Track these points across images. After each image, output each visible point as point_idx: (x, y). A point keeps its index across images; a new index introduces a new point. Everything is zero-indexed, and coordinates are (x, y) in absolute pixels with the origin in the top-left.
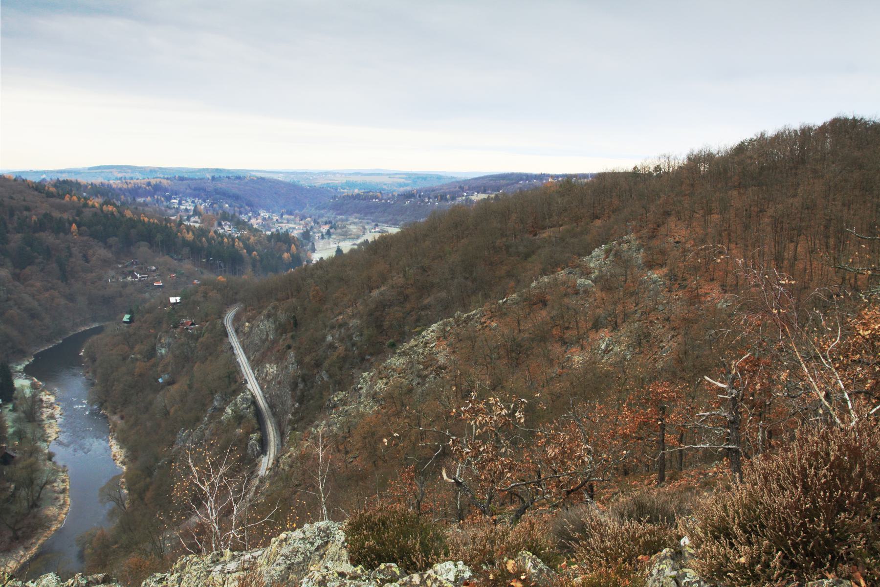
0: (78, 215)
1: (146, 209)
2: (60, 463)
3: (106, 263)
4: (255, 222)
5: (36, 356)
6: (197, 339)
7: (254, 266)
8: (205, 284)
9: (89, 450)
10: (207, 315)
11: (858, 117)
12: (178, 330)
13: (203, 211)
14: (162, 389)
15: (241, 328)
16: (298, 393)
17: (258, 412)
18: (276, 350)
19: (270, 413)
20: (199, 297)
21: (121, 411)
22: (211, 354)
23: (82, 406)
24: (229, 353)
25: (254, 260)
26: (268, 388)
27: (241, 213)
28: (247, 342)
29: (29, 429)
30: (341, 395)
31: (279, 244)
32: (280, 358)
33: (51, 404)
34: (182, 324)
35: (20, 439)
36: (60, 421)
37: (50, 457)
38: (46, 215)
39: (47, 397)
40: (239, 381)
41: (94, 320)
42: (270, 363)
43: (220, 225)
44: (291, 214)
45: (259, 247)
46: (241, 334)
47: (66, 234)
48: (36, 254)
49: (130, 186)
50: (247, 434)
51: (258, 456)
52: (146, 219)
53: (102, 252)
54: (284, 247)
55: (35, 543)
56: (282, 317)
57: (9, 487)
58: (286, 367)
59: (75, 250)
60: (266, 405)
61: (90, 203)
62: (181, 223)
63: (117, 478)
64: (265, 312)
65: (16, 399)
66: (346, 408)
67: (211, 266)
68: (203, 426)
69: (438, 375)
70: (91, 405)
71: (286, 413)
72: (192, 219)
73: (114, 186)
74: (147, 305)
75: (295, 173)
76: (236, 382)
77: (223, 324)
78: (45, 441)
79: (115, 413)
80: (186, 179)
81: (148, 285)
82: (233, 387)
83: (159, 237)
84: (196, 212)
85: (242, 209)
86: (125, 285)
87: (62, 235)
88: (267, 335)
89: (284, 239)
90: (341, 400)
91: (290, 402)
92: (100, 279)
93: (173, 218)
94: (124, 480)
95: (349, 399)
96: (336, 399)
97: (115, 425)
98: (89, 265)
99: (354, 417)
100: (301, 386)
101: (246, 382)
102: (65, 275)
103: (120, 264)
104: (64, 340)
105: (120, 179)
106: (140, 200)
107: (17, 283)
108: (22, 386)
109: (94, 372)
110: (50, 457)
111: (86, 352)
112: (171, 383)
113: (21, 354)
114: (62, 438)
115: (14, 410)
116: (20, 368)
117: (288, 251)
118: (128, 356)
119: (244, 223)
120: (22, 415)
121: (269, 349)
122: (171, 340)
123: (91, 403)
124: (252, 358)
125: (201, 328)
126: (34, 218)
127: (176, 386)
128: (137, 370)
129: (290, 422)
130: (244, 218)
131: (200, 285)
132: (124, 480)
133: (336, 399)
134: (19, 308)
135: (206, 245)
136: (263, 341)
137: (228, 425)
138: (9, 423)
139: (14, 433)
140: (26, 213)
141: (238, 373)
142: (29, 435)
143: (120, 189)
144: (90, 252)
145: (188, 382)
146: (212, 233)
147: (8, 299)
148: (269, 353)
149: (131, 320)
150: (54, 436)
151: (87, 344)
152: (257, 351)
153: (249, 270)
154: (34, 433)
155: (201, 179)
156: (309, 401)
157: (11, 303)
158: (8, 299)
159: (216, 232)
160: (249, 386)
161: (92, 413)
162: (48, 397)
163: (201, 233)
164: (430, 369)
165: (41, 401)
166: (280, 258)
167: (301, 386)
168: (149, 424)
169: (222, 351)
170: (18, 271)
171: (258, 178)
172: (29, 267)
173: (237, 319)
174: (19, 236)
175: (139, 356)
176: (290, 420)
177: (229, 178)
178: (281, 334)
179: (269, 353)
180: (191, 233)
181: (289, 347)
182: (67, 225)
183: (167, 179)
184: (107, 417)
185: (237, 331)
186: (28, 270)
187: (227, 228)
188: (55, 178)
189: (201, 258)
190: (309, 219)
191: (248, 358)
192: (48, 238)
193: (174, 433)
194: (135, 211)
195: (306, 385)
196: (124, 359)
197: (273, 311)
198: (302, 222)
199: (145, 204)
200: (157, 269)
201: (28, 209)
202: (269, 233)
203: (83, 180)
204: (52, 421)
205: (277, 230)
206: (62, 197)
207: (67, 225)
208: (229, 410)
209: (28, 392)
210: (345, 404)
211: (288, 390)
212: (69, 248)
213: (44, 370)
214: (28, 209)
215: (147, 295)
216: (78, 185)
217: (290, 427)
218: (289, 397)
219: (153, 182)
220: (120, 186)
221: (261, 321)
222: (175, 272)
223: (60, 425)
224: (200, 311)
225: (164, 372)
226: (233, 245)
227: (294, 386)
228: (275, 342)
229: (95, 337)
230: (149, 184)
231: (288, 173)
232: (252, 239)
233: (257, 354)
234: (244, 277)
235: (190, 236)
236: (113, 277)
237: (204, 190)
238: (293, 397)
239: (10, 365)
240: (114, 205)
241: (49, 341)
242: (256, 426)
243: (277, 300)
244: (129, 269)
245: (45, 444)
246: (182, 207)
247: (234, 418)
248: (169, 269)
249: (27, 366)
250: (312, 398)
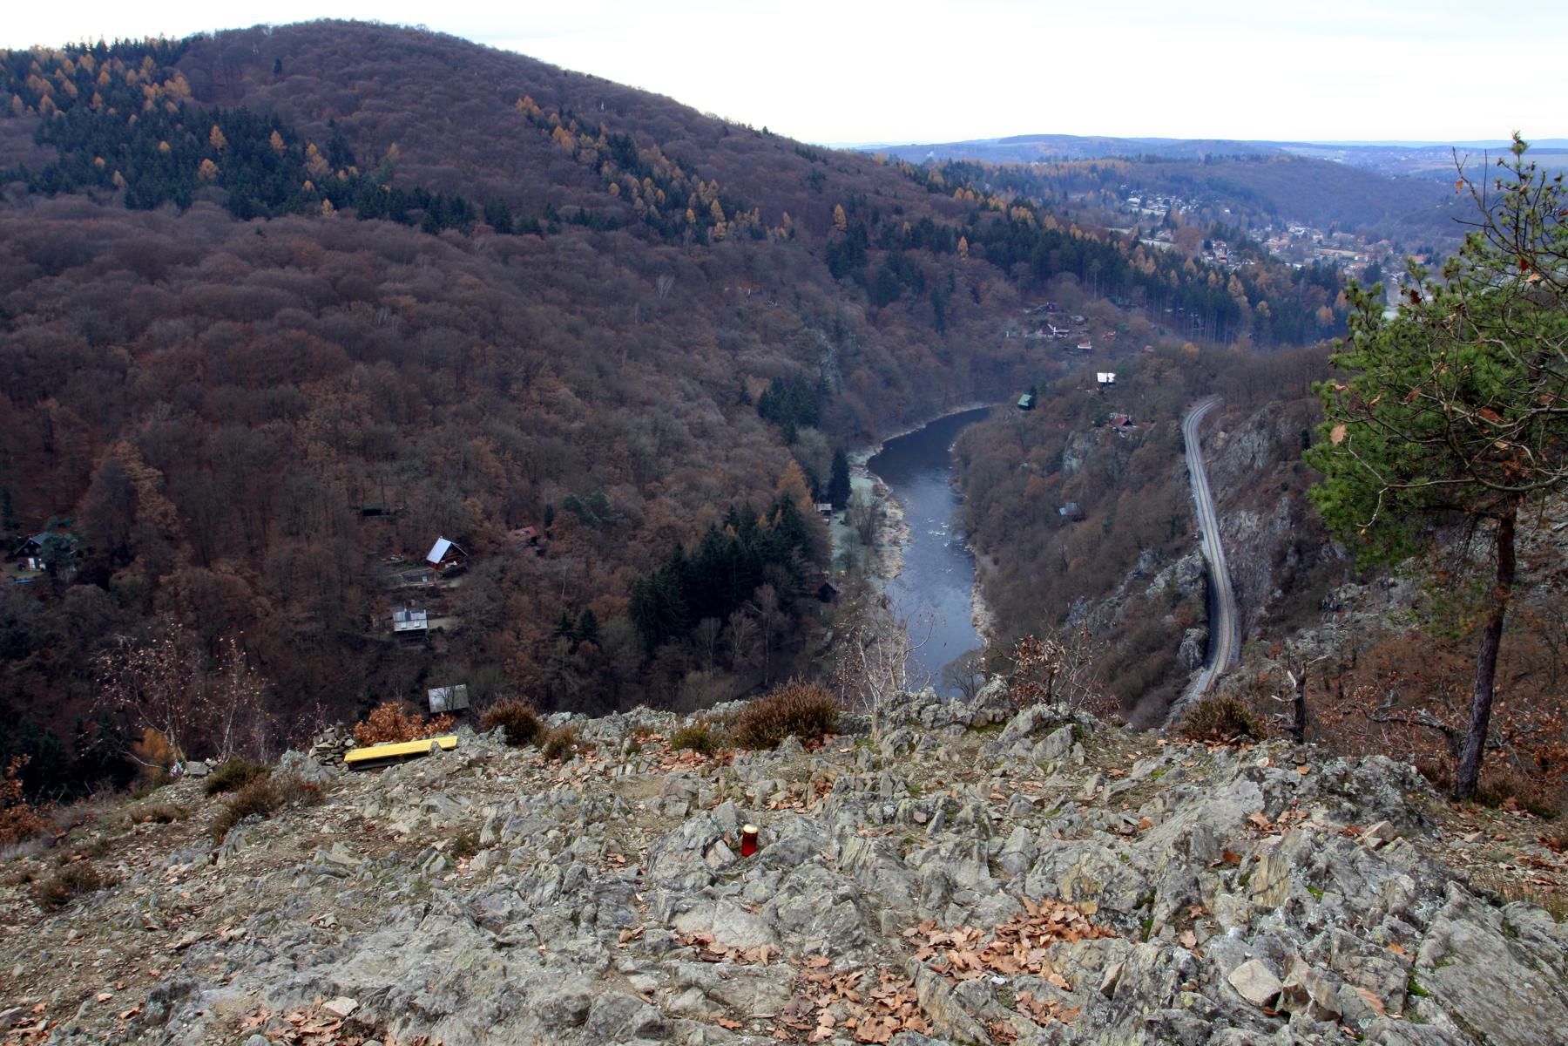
0: (971, 224)
1: (1083, 213)
3: (1005, 304)
4: (1275, 245)
5: (887, 445)
6: (1132, 451)
10: (1154, 410)
11: (122, 41)
12: (1103, 430)
13: (1180, 221)
15: (1210, 440)
16: (1285, 572)
17: (1210, 596)
18: (1263, 487)
19: (1231, 599)
20: (1146, 378)
23: (941, 533)
24: (1182, 481)
25: (1260, 318)
26: (1237, 553)
27: (1251, 226)
28: (1216, 466)
29: (861, 553)
30: (1355, 590)
31: (1314, 288)
32: (1267, 505)
33: (898, 522)
35: (849, 568)
36: (906, 550)
37: (884, 603)
38: (923, 222)
39: (893, 511)
41: (977, 398)
42: (1249, 510)
43: (1208, 246)
44: (1349, 230)
45: (1273, 293)
46: (1208, 450)
47: (950, 253)
49: (1062, 172)
50: (1184, 626)
51: (1194, 668)
52: (1078, 233)
53: (1001, 286)
54: (1324, 295)
56: (1285, 430)
58: (1271, 523)
59: (960, 281)
60: (1228, 584)
61: (992, 203)
62: (1136, 243)
63: (972, 654)
64: (1256, 417)
66: (1359, 615)
67: (1180, 324)
68: (1115, 599)
69: (1557, 586)
71: (1258, 603)
72: (1160, 234)
73: (1036, 172)
74: (1059, 383)
75: (957, 147)
77: (1179, 429)
78: (880, 577)
80: (1159, 160)
81: (1068, 347)
82: (1178, 542)
83: (1096, 265)
84: (1168, 223)
85: (1255, 219)
87: (944, 253)
89: (1325, 279)
90: (1352, 599)
91: (1266, 586)
92: (993, 331)
93: (1126, 232)
95: (1369, 601)
96: (1342, 595)
97: (984, 571)
99: (1370, 635)
100: (1292, 561)
101: (1201, 537)
102: (942, 321)
105: (1048, 160)
106: (1075, 197)
107: (872, 329)
109: (965, 482)
110: (884, 603)
112: (1078, 518)
113: (867, 439)
114: (904, 577)
115: (846, 522)
116: (863, 459)
117: (1330, 302)
118: (1019, 463)
119: (1254, 246)
120: (856, 532)
121: (1253, 485)
122: (1088, 446)
123: (954, 530)
124: (1220, 497)
125: (1140, 433)
126: (907, 226)
127: (1084, 524)
129: (1261, 621)
130: (1255, 235)
131: (1152, 355)
133: (1342, 595)
135: (1175, 283)
136: (1245, 470)
137: (1155, 605)
138: (836, 541)
139: (842, 557)
140: (895, 217)
142: (861, 565)
143: (1045, 178)
144: (984, 285)
145: (1105, 522)
146: (1189, 263)
148: (1250, 493)
149: (1031, 405)
150: (895, 572)
151: (960, 437)
152: (1231, 485)
153: (1245, 335)
154: (867, 563)
155: (1185, 161)
156: (1301, 590)
157: (860, 358)
159: (1196, 261)
160: (1205, 546)
161: (954, 546)
163: (1173, 260)
164: (1542, 572)
165: (884, 515)
166: (1312, 316)
167: (1292, 561)
169: (1170, 477)
170: (875, 309)
171: (1293, 159)
172: (891, 305)
173: (1207, 422)
174: (882, 254)
175: (1035, 466)
176: (1262, 618)
177: (1237, 158)
178: (1278, 460)
179: (1250, 493)
180: (1151, 260)
181: (1285, 488)
182: (953, 239)
183: (1127, 160)
184: (973, 557)
185: (1202, 445)
186: (889, 309)
187: (1219, 253)
188: (946, 157)
190: (1384, 242)
191: (1214, 496)
192: (923, 258)
194: (1064, 218)
195: (1301, 560)
197: (1270, 417)
198: (1371, 248)
199: (1083, 205)
201: (899, 211)
203: (988, 162)
204: (896, 548)
205: (1316, 262)
206: (950, 191)
207: (953, 239)
208: (1160, 581)
209: (867, 500)
210: (1359, 608)
211: (1267, 563)
212: (951, 277)
214: (899, 211)
215: (1064, 365)
216: (979, 171)
217: (1258, 630)
218: (1268, 576)
219: (1101, 165)
220: (1046, 171)
221: (1246, 432)
222: (1115, 328)
223: (905, 557)
225: (1070, 498)
227: (1281, 558)
228: (1262, 474)
230: (1093, 169)
231: (1355, 149)
232: (1263, 278)
233: (1231, 491)
234: (1234, 348)
235: (1148, 267)
237: (1189, 181)
238: (1273, 577)
240: (1029, 206)
241: (907, 422)
242: (1202, 616)
243: (1281, 397)
244: (1041, 317)
246: (1146, 211)
248: (1106, 323)
249: (872, 458)
250: (1309, 586)
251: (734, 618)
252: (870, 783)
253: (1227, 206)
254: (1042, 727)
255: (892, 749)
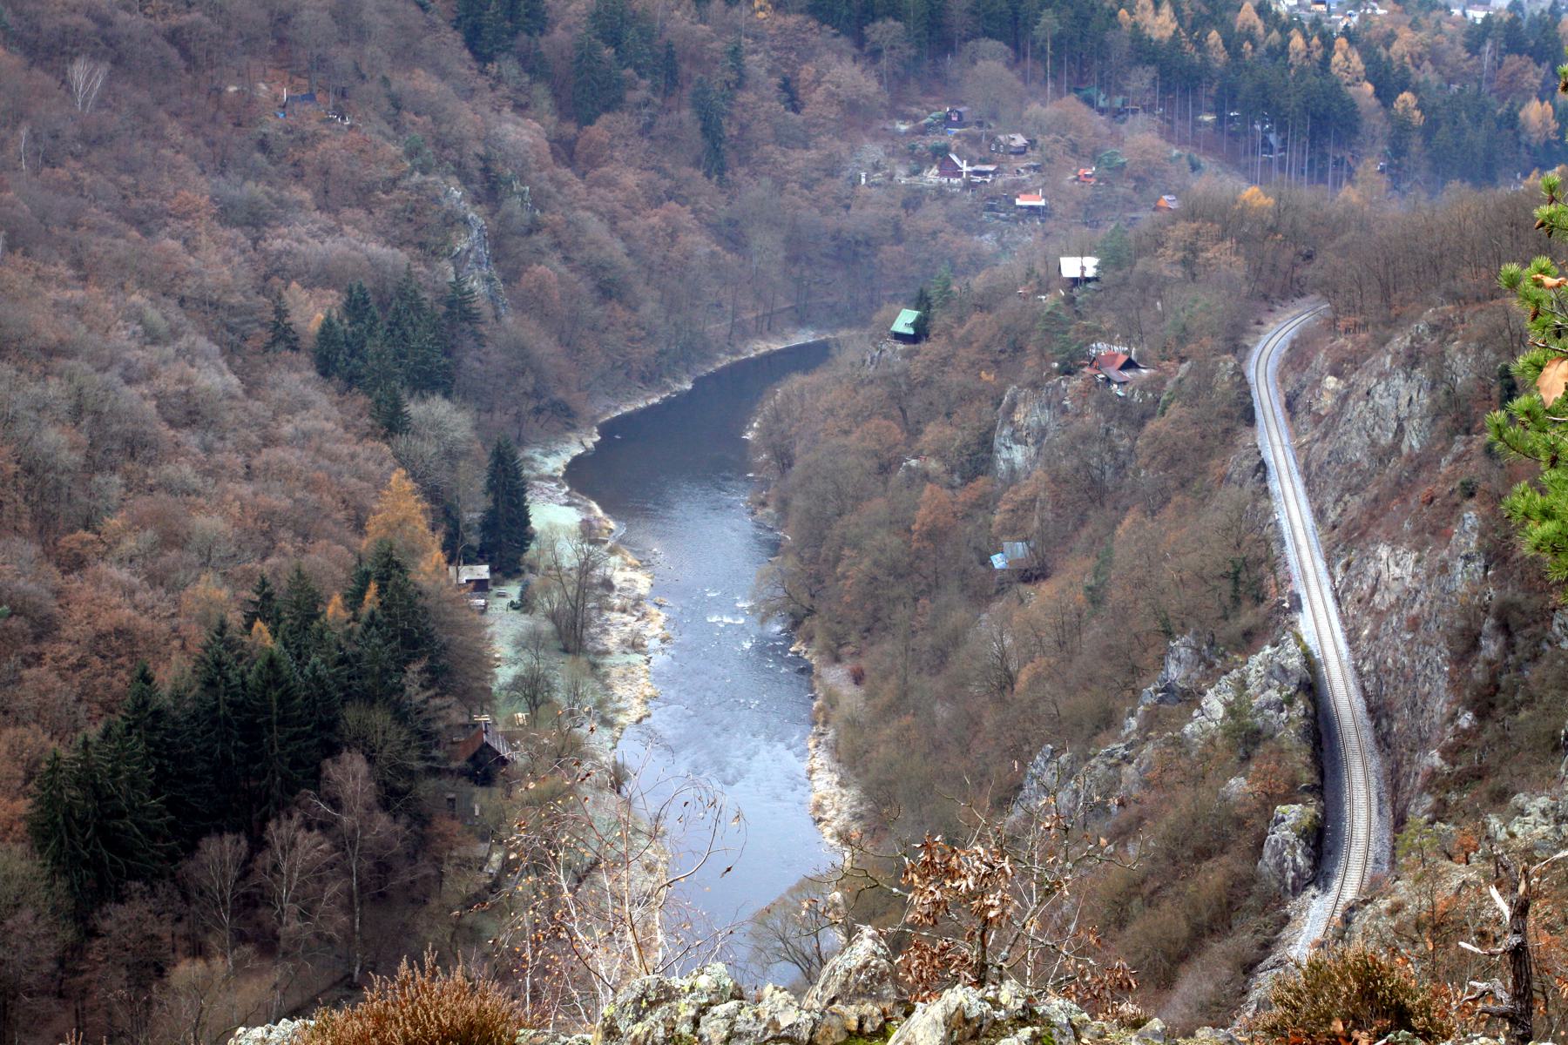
2: (646, 808)
5: (607, 430)
6: (1140, 423)
7: (1398, 150)
8: (1192, 214)
9: (740, 775)
10: (1184, 335)
12: (1077, 382)
14: (1000, 591)
15: (1306, 396)
16: (1479, 674)
17: (1321, 731)
18: (1423, 491)
19: (1368, 736)
20: (1165, 264)
21: (858, 654)
22: (1183, 484)
24: (1250, 486)
25: (1402, 128)
26: (1374, 637)
28: (1321, 451)
29: (561, 672)
31: (1513, 62)
33: (638, 601)
34: (1093, 361)
35: (534, 705)
36: (659, 660)
37: (618, 778)
40: (1273, 597)
41: (801, 322)
42: (1394, 542)
45: (1427, 74)
46: (1303, 417)
48: (630, 71)
50: (1270, 800)
51: (1297, 890)
54: (1534, 75)
55: (848, 993)
57: (487, 860)
58: (1444, 568)
59: (756, 63)
60: (1360, 704)
63: (812, 884)
64: (1400, 342)
65: (533, 568)
67: (1233, 146)
68: (1119, 748)
70: (763, 621)
71: (1423, 743)
74: (978, 282)
76: (1259, 599)
77: (1240, 373)
78: (607, 723)
79: (837, 659)
82: (1248, 617)
86: (914, 200)
88: (1401, 430)
91: (1440, 706)
94: (837, 896)
97: (832, 700)
98: (798, 119)
100: (1491, 647)
101: (1297, 604)
102: (718, 152)
103: (905, 118)
104: (698, 382)
107: (565, 173)
108: (553, 528)
109: (784, 505)
111: (766, 432)
112: (1032, 574)
113: (564, 418)
114: (660, 720)
116: (555, 464)
120: (547, 627)
121: (1401, 488)
122: (1046, 417)
124: (1332, 516)
125: (1157, 384)
127: (1046, 588)
128: (923, 511)
131: (1175, 217)
132: (837, 896)
134: (566, 259)
136: (1383, 456)
138: (502, 648)
139: (517, 684)
141: (1273, 570)
142: (560, 697)
145: (1089, 581)
147: (533, 228)
148: (1395, 505)
149: (920, 333)
150: (637, 711)
152: (1354, 490)
153: (1371, 167)
156: (1515, 710)
157: (542, 239)
158: (533, 228)
161: (764, 649)
162: (629, 574)
165: (608, 585)
166: (1511, 120)
167: (1491, 647)
168: (942, 712)
169: (1225, 479)
170: (570, 129)
172: (605, 118)
173: (1298, 356)
175: (933, 465)
176: (1434, 774)
179: (1395, 505)
181: (1469, 492)
184: (807, 670)
185: (1290, 405)
186: (599, 130)
189: (1198, 109)
191: (1319, 514)
193: (1020, 752)
195: (1510, 646)
196: (885, 469)
197: (1431, 342)
200: (1032, 143)
202: (1477, 15)
204: (636, 658)
208: (1215, 703)
209: (568, 553)
211: (1439, 655)
212: (736, 53)
213: (622, 477)
215: (988, 242)
217: (1429, 801)
218: (1442, 683)
221: (1384, 375)
222: (1094, 157)
224: (1162, 317)
225: (1012, 531)
226: (1325, 62)
227: (1469, 642)
228: (1422, 463)
229: (797, 381)
233: (1355, 502)
234: (1350, 194)
236: (876, 167)
238: (1455, 685)
239: (527, 452)
241: (650, 379)
242: (1307, 777)
243: (1454, 297)
244: (933, 140)
245: (605, 734)
247: (1229, 733)
248: (1074, 148)
249: (577, 460)
250: (1529, 701)
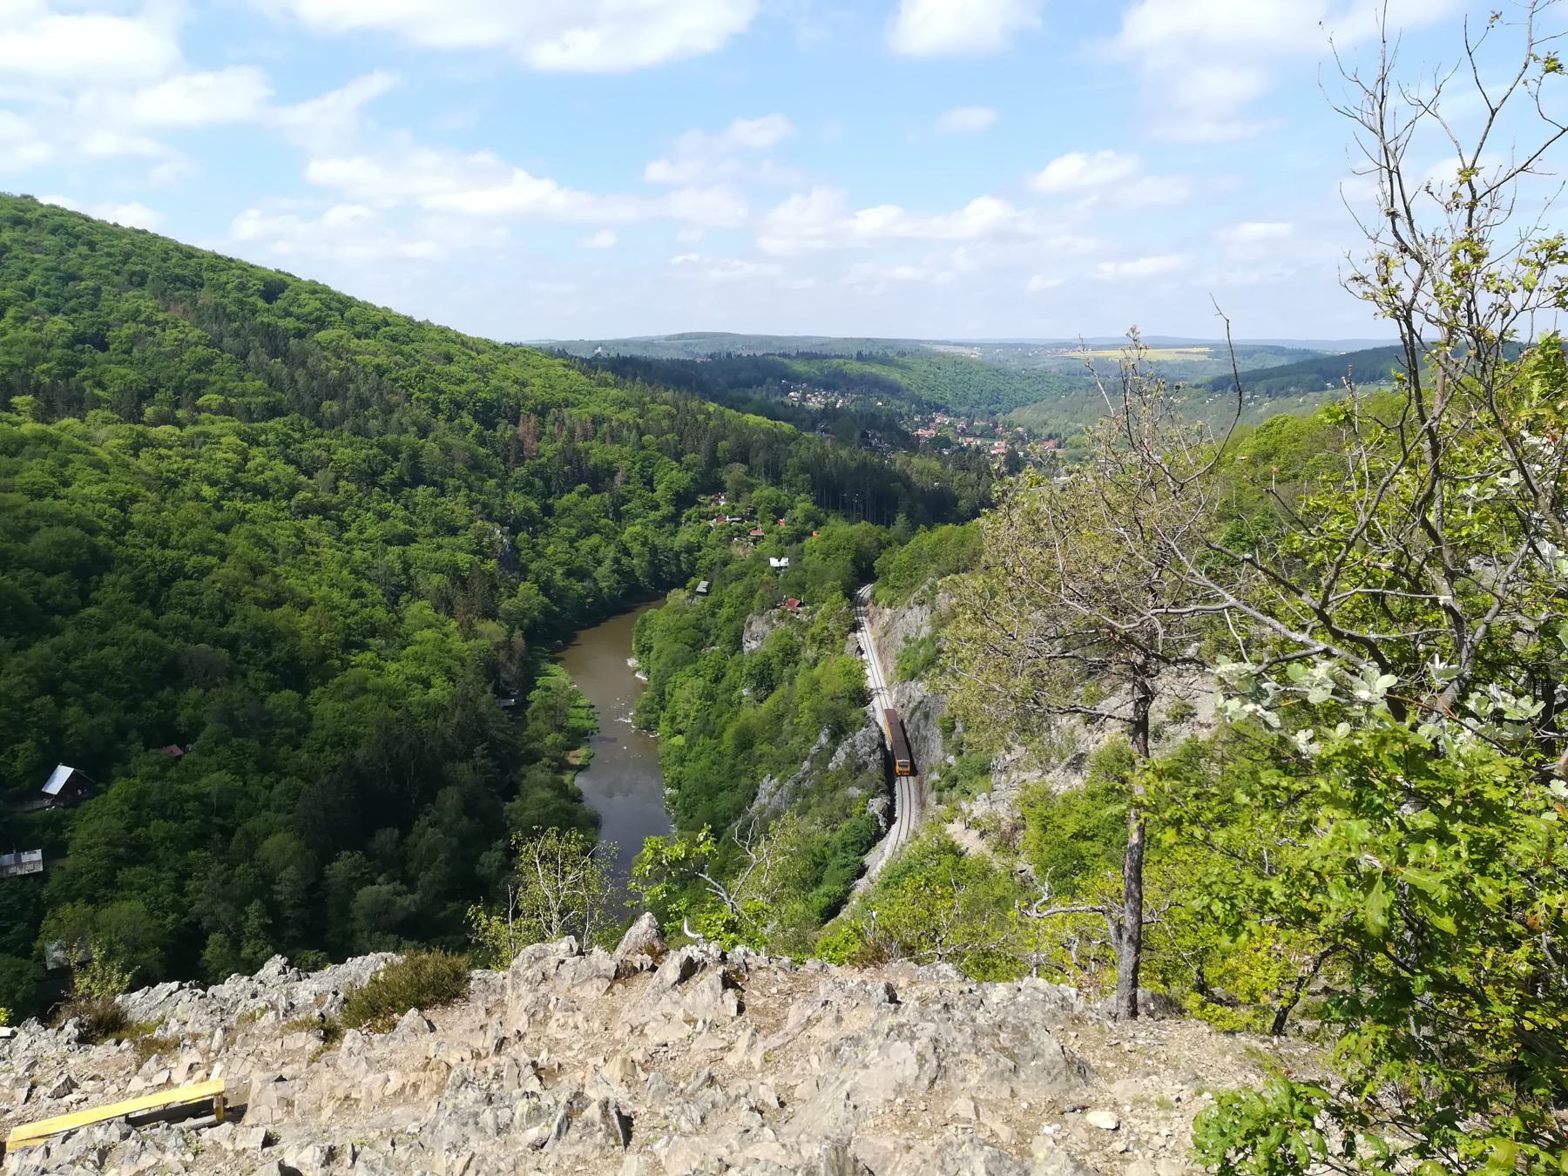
75: (626, 343)
122: (766, 628)
188: (613, 354)
251: (417, 827)
252: (492, 1071)
253: (879, 399)
254: (689, 969)
255: (525, 1018)
